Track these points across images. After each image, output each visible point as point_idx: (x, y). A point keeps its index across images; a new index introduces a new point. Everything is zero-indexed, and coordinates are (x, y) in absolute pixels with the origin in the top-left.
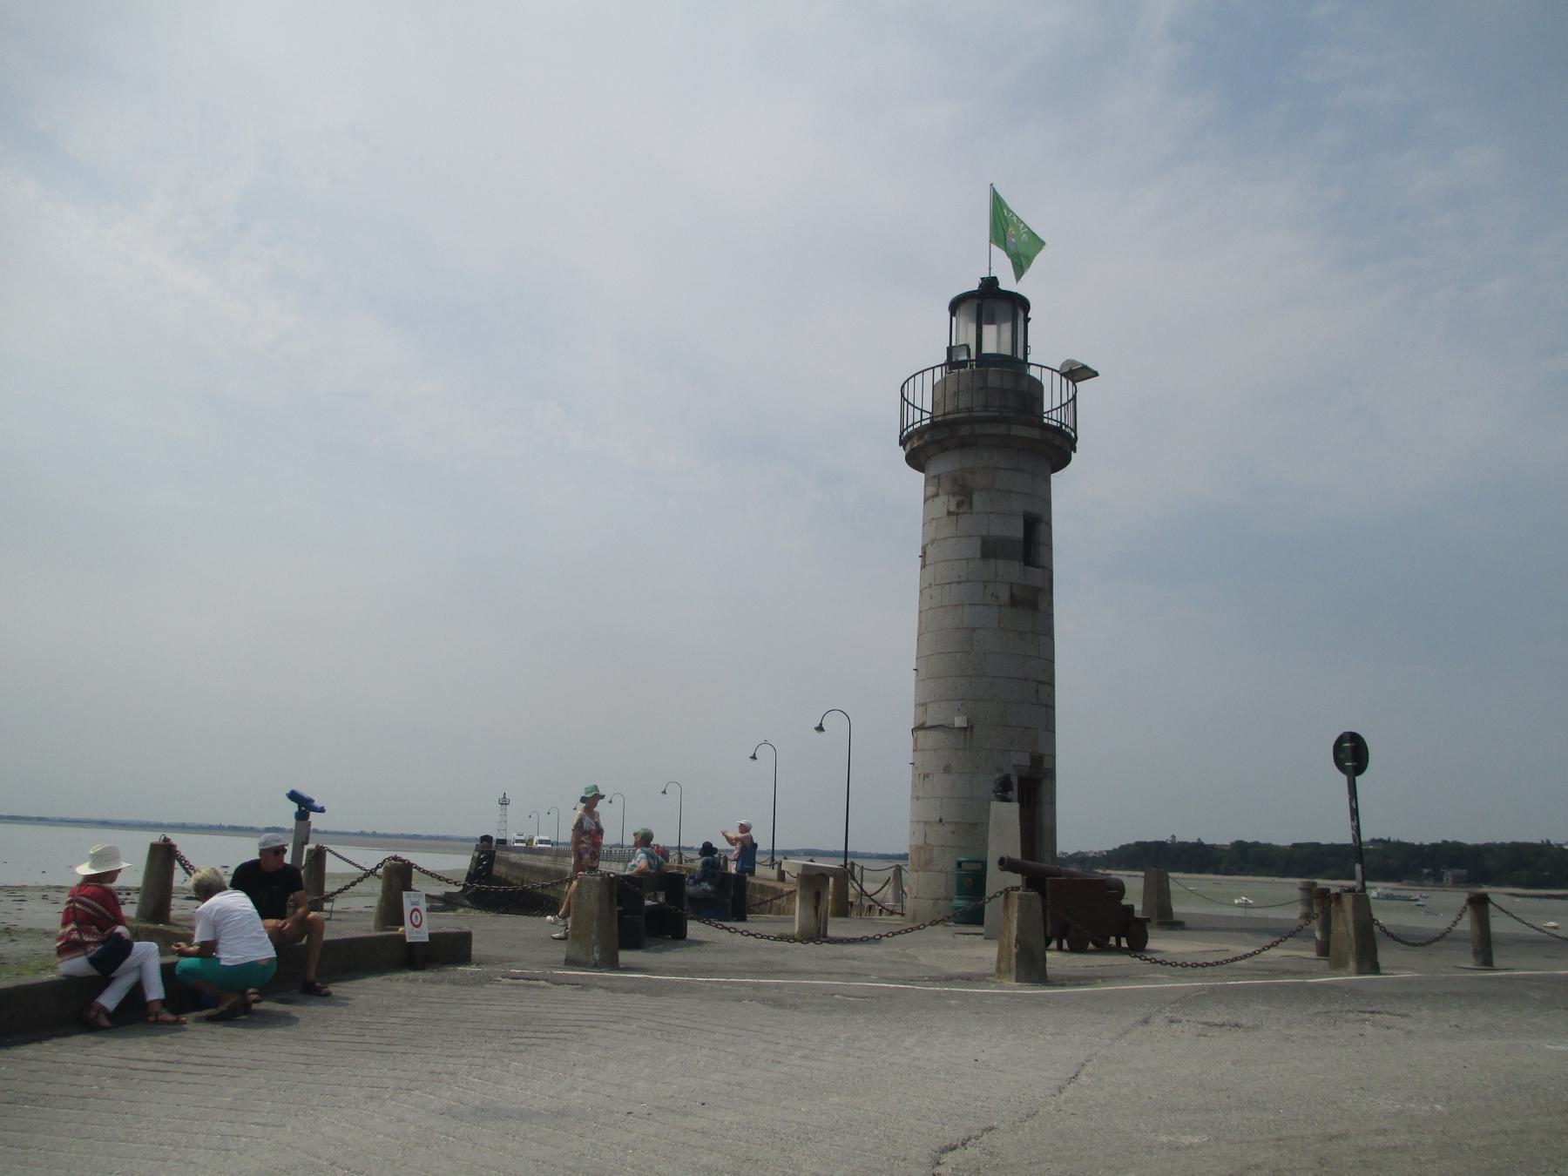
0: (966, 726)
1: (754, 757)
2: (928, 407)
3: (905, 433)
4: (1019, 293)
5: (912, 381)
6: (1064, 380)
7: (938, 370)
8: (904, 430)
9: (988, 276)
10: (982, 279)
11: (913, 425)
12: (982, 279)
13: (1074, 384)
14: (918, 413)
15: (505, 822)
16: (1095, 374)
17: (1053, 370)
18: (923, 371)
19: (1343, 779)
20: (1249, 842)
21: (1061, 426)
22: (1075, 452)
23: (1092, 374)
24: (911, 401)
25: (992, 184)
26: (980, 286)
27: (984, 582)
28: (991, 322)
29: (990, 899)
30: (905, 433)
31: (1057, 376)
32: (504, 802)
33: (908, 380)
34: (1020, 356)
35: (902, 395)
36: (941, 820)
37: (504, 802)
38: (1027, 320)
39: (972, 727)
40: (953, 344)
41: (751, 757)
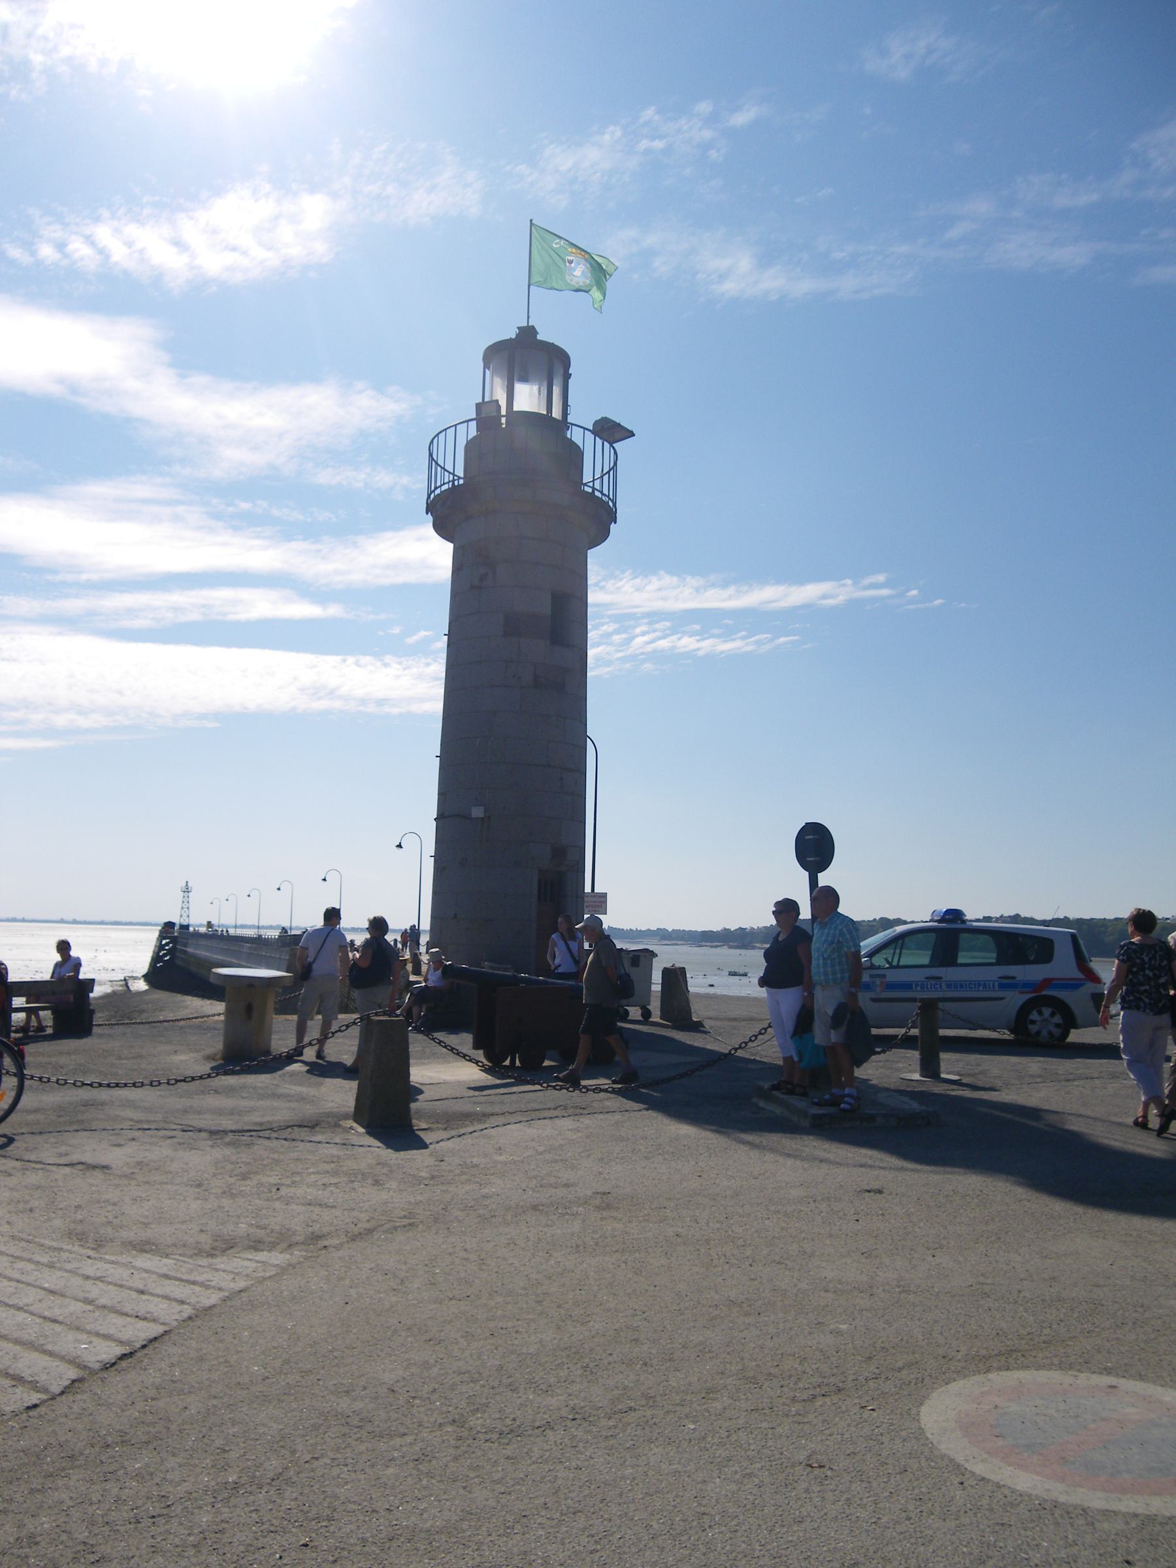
0: (483, 816)
1: (400, 846)
2: (460, 472)
3: (432, 496)
4: (556, 343)
5: (442, 436)
6: (599, 441)
7: (462, 429)
8: (431, 493)
9: (526, 325)
10: (518, 328)
11: (441, 485)
12: (518, 328)
13: (611, 445)
14: (451, 476)
15: (188, 908)
16: (631, 434)
17: (585, 429)
18: (446, 430)
19: (805, 875)
20: (891, 918)
21: (593, 492)
22: (615, 523)
23: (629, 435)
24: (441, 462)
25: (531, 221)
26: (517, 335)
28: (524, 379)
29: (333, 1033)
30: (432, 496)
31: (590, 437)
32: (187, 890)
33: (437, 435)
34: (556, 413)
35: (431, 455)
36: (455, 916)
37: (187, 890)
38: (567, 376)
39: (489, 818)
40: (487, 399)
41: (398, 846)
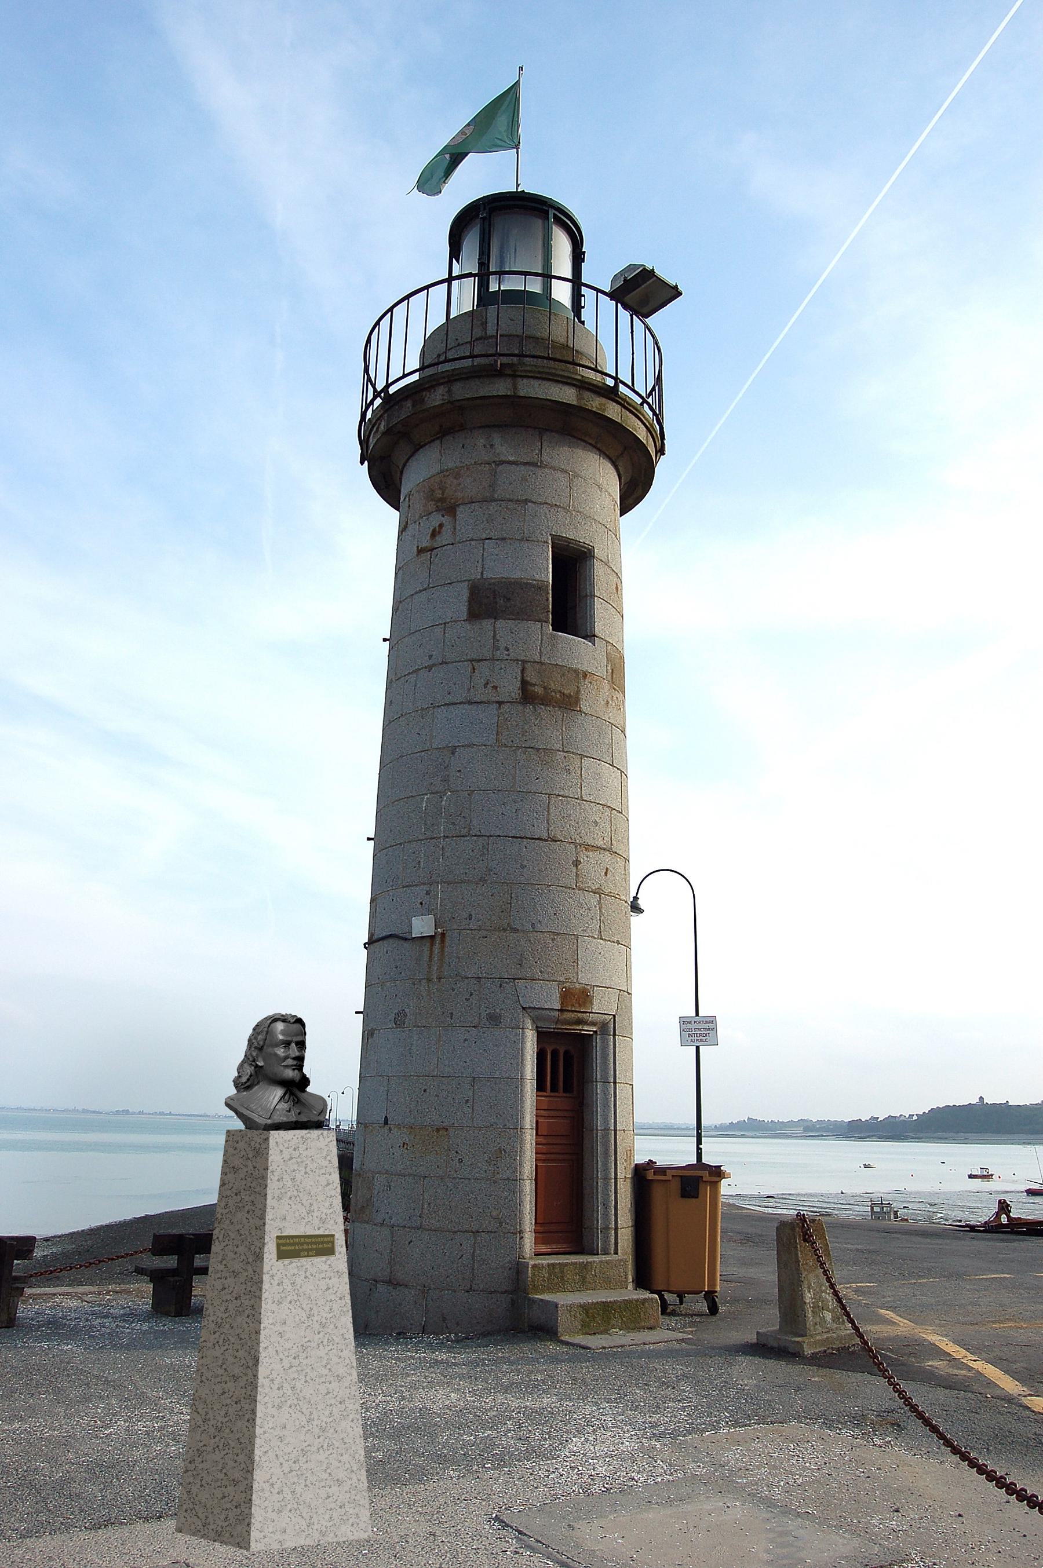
27: (471, 661)
39: (443, 935)
